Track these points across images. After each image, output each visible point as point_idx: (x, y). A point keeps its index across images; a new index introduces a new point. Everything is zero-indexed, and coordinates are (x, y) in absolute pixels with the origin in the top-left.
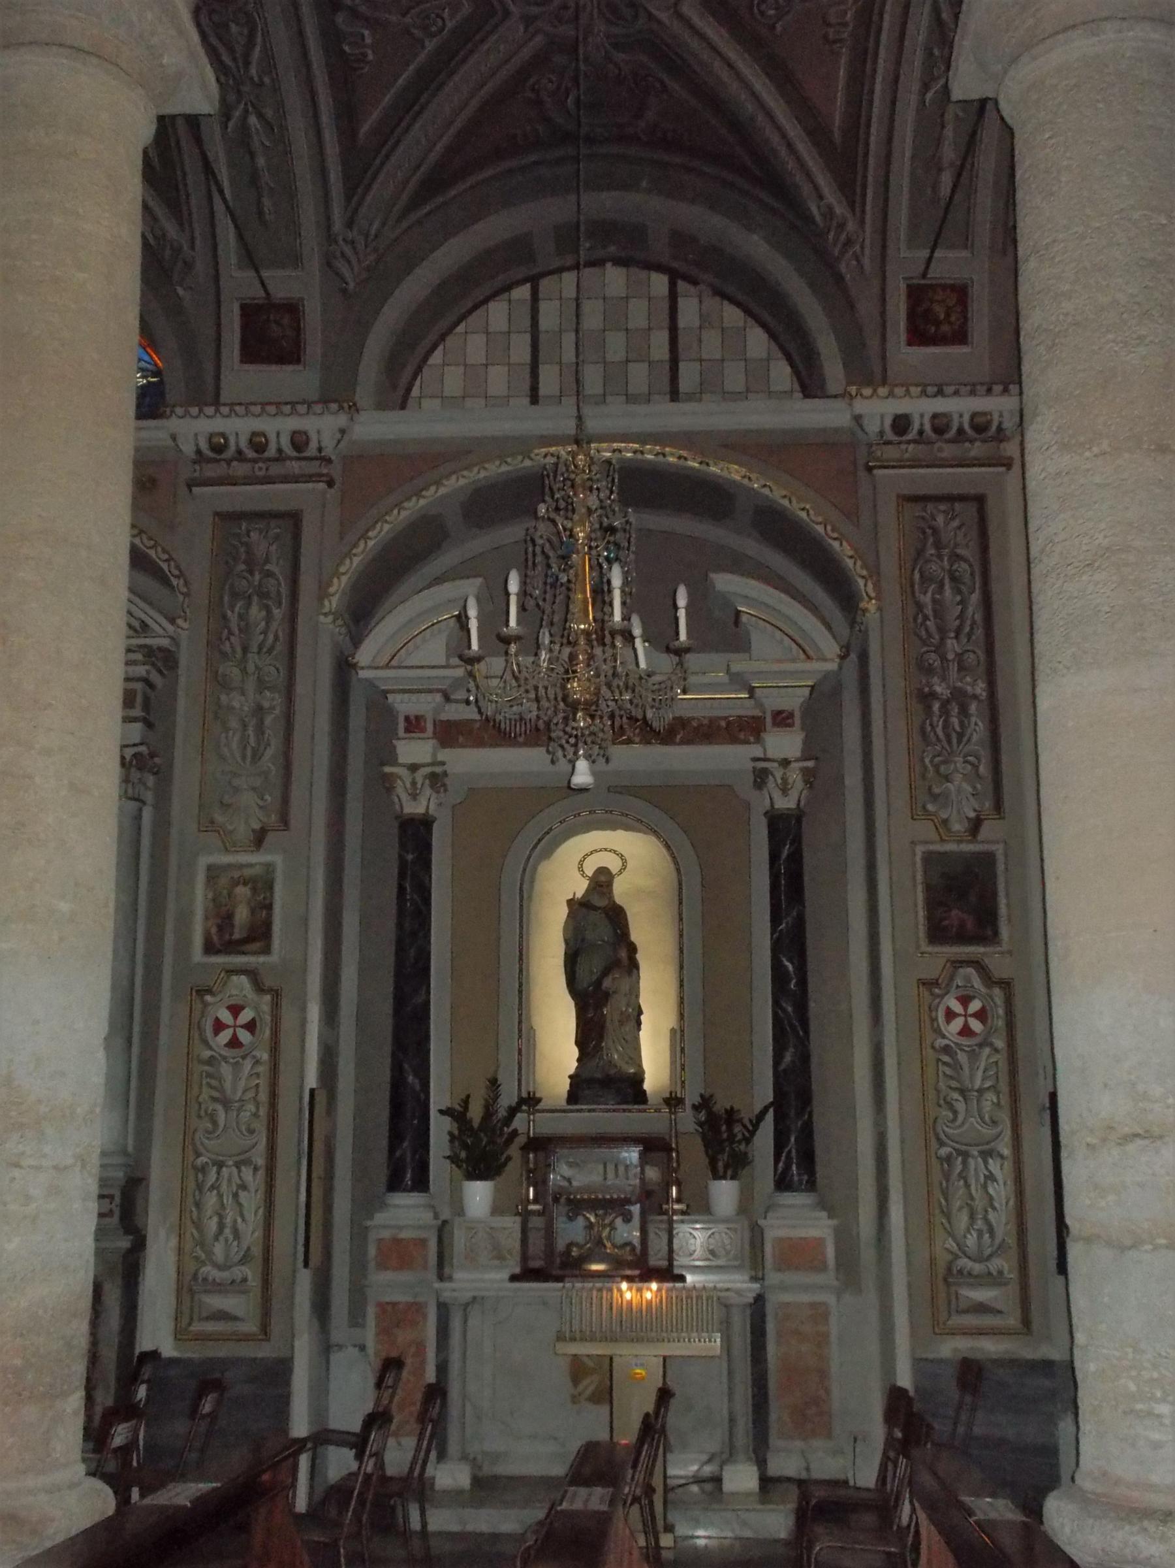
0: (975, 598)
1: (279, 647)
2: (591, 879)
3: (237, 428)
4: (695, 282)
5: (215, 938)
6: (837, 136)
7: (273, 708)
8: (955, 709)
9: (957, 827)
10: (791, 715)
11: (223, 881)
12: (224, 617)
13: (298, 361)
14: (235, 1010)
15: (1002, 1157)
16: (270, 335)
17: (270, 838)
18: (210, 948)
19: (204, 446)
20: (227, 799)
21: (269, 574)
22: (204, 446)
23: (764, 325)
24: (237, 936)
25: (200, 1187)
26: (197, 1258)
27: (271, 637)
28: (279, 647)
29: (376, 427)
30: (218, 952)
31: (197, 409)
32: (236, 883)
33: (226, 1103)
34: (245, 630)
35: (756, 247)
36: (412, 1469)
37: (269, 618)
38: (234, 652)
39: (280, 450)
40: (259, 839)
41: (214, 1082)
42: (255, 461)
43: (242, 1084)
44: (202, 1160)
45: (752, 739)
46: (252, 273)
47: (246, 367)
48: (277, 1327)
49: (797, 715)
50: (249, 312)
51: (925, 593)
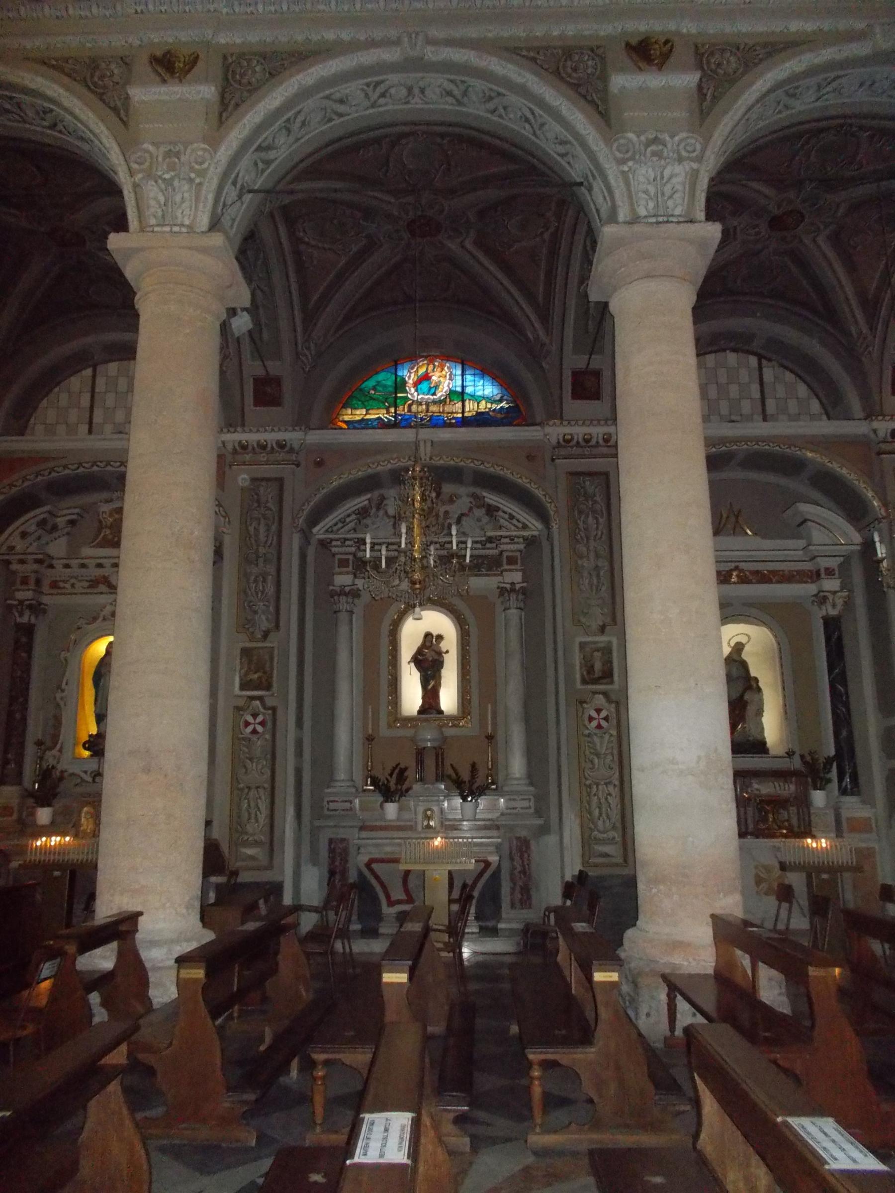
0: (274, 528)
2: (733, 648)
3: (579, 431)
4: (769, 360)
6: (541, 299)
8: (594, 573)
9: (259, 636)
10: (834, 570)
11: (588, 649)
12: (576, 523)
13: (598, 399)
14: (598, 711)
16: (267, 392)
17: (608, 628)
18: (584, 682)
19: (561, 440)
20: (585, 611)
22: (561, 440)
23: (805, 382)
24: (596, 676)
25: (589, 794)
26: (590, 828)
27: (600, 533)
29: (315, 437)
30: (587, 683)
33: (598, 755)
35: (813, 346)
37: (597, 523)
39: (597, 442)
40: (602, 629)
43: (605, 745)
44: (241, 786)
46: (259, 363)
48: (276, 862)
49: (837, 569)
50: (257, 380)
51: (251, 525)
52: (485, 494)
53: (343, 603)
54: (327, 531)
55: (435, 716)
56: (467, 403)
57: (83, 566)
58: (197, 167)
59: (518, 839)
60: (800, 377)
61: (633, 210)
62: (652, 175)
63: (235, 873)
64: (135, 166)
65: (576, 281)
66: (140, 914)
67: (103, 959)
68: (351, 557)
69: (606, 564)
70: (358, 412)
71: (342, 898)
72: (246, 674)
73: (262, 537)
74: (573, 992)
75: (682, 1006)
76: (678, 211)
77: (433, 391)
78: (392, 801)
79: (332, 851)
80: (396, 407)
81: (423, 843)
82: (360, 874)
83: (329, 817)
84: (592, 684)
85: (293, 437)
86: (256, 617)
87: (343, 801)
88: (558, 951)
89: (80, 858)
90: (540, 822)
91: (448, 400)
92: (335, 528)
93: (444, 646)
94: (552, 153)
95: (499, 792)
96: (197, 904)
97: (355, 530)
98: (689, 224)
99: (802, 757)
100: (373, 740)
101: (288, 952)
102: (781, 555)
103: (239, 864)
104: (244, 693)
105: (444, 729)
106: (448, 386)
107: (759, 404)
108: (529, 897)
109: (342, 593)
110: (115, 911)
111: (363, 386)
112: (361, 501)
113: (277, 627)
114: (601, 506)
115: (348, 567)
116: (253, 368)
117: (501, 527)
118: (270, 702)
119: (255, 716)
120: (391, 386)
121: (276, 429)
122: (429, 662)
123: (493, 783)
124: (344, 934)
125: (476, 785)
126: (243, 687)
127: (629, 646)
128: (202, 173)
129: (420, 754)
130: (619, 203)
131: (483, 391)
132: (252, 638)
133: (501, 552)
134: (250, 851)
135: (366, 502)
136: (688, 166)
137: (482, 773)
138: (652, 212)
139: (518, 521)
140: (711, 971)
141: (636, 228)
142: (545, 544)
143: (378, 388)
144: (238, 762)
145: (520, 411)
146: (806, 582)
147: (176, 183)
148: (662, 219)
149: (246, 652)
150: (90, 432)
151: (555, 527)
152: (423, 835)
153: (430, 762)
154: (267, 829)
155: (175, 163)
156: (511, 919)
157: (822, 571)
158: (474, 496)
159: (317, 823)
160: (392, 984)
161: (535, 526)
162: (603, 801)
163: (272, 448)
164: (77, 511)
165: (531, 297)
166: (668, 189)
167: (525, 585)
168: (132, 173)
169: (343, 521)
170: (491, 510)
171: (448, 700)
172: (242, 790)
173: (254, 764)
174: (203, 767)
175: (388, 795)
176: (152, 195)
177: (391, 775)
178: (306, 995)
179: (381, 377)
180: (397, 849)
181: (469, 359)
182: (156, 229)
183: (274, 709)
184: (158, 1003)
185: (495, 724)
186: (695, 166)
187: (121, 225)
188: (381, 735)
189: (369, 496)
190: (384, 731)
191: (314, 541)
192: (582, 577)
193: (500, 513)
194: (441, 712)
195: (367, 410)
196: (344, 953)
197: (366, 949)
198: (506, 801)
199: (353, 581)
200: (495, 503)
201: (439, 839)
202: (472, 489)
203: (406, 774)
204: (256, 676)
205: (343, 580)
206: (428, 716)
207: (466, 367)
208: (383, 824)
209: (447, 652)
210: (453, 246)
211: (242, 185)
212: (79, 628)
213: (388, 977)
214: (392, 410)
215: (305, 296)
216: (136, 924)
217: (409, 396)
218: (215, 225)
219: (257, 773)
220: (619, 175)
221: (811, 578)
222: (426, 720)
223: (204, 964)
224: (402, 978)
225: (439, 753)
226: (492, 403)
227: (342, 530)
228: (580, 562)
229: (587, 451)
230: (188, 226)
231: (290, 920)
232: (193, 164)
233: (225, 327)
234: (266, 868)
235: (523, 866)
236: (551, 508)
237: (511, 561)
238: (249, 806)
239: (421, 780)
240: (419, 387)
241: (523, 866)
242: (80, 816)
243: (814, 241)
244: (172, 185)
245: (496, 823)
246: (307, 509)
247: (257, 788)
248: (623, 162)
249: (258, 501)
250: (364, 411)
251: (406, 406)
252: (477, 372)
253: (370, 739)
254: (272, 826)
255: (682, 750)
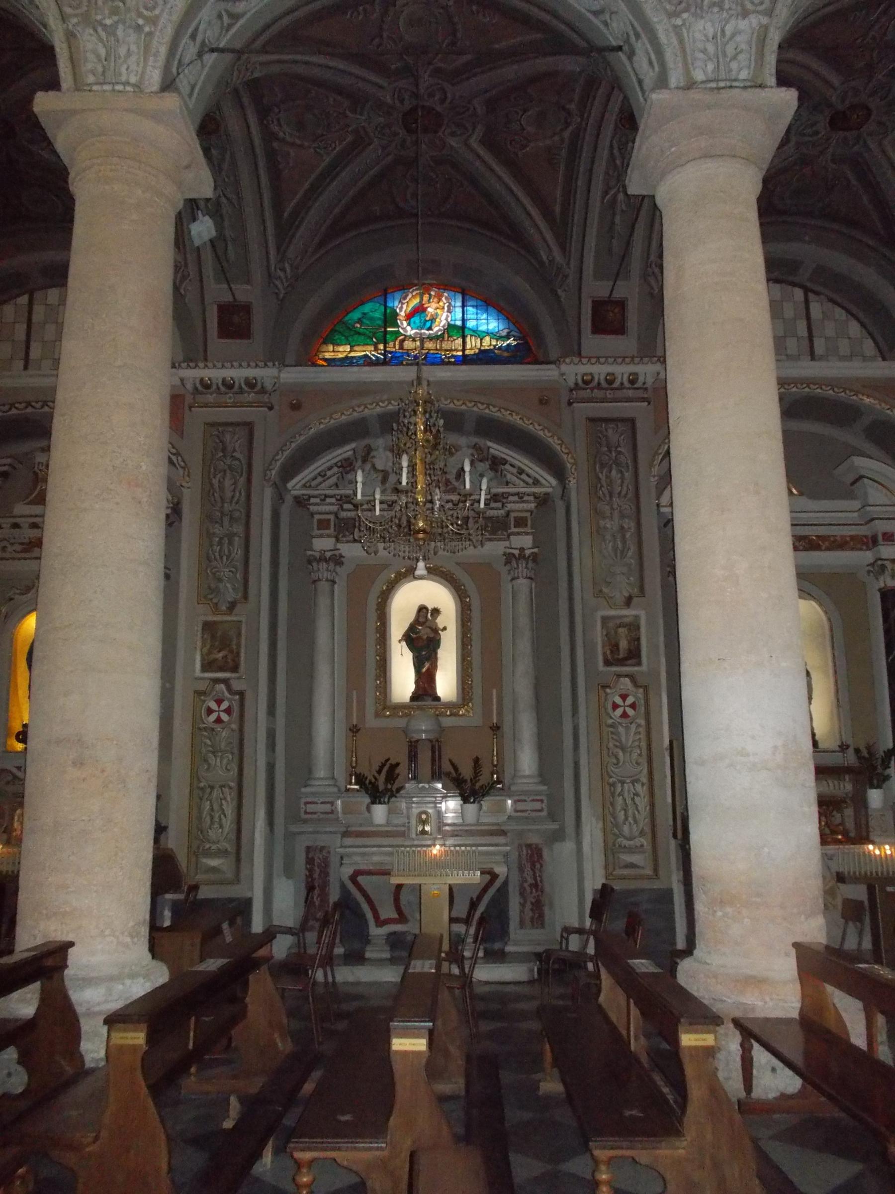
0: (242, 480)
1: (630, 495)
3: (600, 371)
5: (609, 657)
6: (558, 209)
7: (629, 528)
8: (619, 536)
11: (611, 625)
14: (624, 697)
15: (230, 788)
16: (234, 322)
17: (635, 600)
18: (607, 663)
19: (580, 381)
20: (608, 580)
21: (620, 453)
22: (580, 381)
24: (621, 656)
25: (613, 794)
26: (614, 834)
27: (625, 488)
28: (630, 495)
29: (291, 375)
31: (578, 359)
32: (620, 626)
33: (623, 749)
34: (610, 483)
36: (332, 971)
37: (623, 478)
38: (605, 496)
39: (622, 384)
40: (628, 602)
41: (615, 737)
42: (606, 389)
44: (202, 785)
45: (864, 548)
46: (225, 286)
47: (596, 336)
48: (244, 872)
52: (490, 444)
53: (323, 571)
54: (304, 486)
55: (429, 702)
56: (468, 339)
57: (16, 526)
58: (146, 13)
59: (529, 846)
60: (853, 315)
61: (687, 72)
62: (711, 32)
63: (195, 888)
64: (68, 10)
65: (599, 193)
66: (71, 944)
67: (24, 1004)
68: (332, 517)
69: (633, 525)
70: (341, 349)
71: (325, 922)
72: (210, 652)
73: (229, 494)
74: (633, 1048)
75: (761, 1056)
76: (744, 75)
77: (428, 325)
78: (380, 803)
79: (310, 861)
80: (385, 343)
81: (425, 852)
82: (343, 886)
83: (305, 821)
84: (617, 665)
85: (265, 374)
86: (221, 586)
87: (322, 803)
88: (599, 991)
89: (10, 870)
90: (555, 826)
91: (446, 336)
92: (314, 483)
93: (440, 622)
94: (583, 11)
95: (506, 792)
96: (145, 931)
97: (337, 485)
98: (758, 90)
99: (857, 751)
100: (358, 730)
101: (260, 990)
102: (828, 517)
103: (200, 877)
104: (207, 675)
105: (440, 718)
106: (446, 319)
107: (806, 343)
108: (541, 916)
109: (323, 559)
110: (39, 941)
111: (347, 318)
112: (345, 451)
113: (246, 597)
114: (626, 458)
115: (330, 529)
116: (217, 292)
117: (507, 483)
118: (237, 686)
119: (219, 702)
120: (380, 319)
121: (244, 364)
122: (423, 641)
123: (499, 782)
124: (328, 961)
125: (478, 785)
126: (206, 667)
127: (680, 608)
128: (154, 21)
129: (413, 748)
130: (670, 65)
131: (487, 326)
132: (216, 607)
133: (508, 514)
134: (214, 862)
135: (351, 453)
136: (754, 20)
137: (486, 770)
138: (711, 76)
139: (528, 476)
140: (795, 1014)
141: (694, 95)
142: (560, 506)
143: (364, 321)
144: (199, 759)
145: (529, 350)
146: (861, 549)
147: (120, 32)
148: (721, 84)
149: (208, 627)
150: (26, 368)
151: (572, 483)
152: (416, 843)
153: (425, 756)
154: (233, 836)
155: (118, 7)
156: (521, 939)
157: (880, 538)
158: (476, 447)
159: (294, 828)
160: (405, 1053)
161: (549, 483)
162: (629, 802)
163: (240, 387)
164: (9, 461)
165: (547, 214)
166: (730, 50)
167: (536, 550)
168: (64, 18)
169: (322, 474)
170: (496, 464)
171: (446, 684)
172: (202, 789)
173: (218, 760)
174: (151, 761)
175: (376, 795)
176: (90, 46)
177: (379, 772)
178: (284, 1046)
179: (367, 308)
180: (388, 859)
181: (471, 290)
182: (95, 88)
183: (241, 694)
184: (93, 1059)
185: (500, 713)
186: (765, 20)
187: (53, 84)
188: (367, 726)
189: (353, 445)
190: (371, 722)
191: (289, 499)
192: (604, 540)
193: (507, 467)
194: (438, 699)
195: (352, 347)
196: (326, 983)
197: (351, 979)
198: (515, 802)
199: (335, 545)
200: (503, 456)
201: (438, 847)
202: (475, 440)
203: (397, 771)
204: (221, 655)
205: (323, 544)
206: (423, 703)
207: (467, 297)
208: (369, 829)
209: (445, 629)
210: (453, 142)
211: (204, 41)
212: (11, 599)
213: (399, 1044)
214: (381, 346)
215: (278, 207)
216: (65, 958)
217: (401, 330)
218: (168, 85)
219: (221, 769)
220: (671, 29)
221: (867, 544)
222: (419, 708)
223: (144, 1026)
224: (420, 1044)
225: (436, 747)
226: (497, 340)
227: (323, 485)
228: (602, 523)
229: (609, 394)
230: (133, 85)
231: (262, 952)
232: (142, 10)
233: (181, 239)
234: (230, 883)
235: (535, 879)
236: (568, 460)
237: (520, 522)
238: (212, 809)
239: (415, 778)
240: (412, 320)
241: (535, 879)
242: (13, 818)
243: (880, 144)
244: (115, 35)
245: (503, 828)
246: (282, 458)
247: (222, 786)
248: (676, 14)
249: (224, 450)
250: (348, 348)
251: (397, 343)
252: (480, 303)
253: (354, 730)
254: (239, 831)
255: (753, 737)
